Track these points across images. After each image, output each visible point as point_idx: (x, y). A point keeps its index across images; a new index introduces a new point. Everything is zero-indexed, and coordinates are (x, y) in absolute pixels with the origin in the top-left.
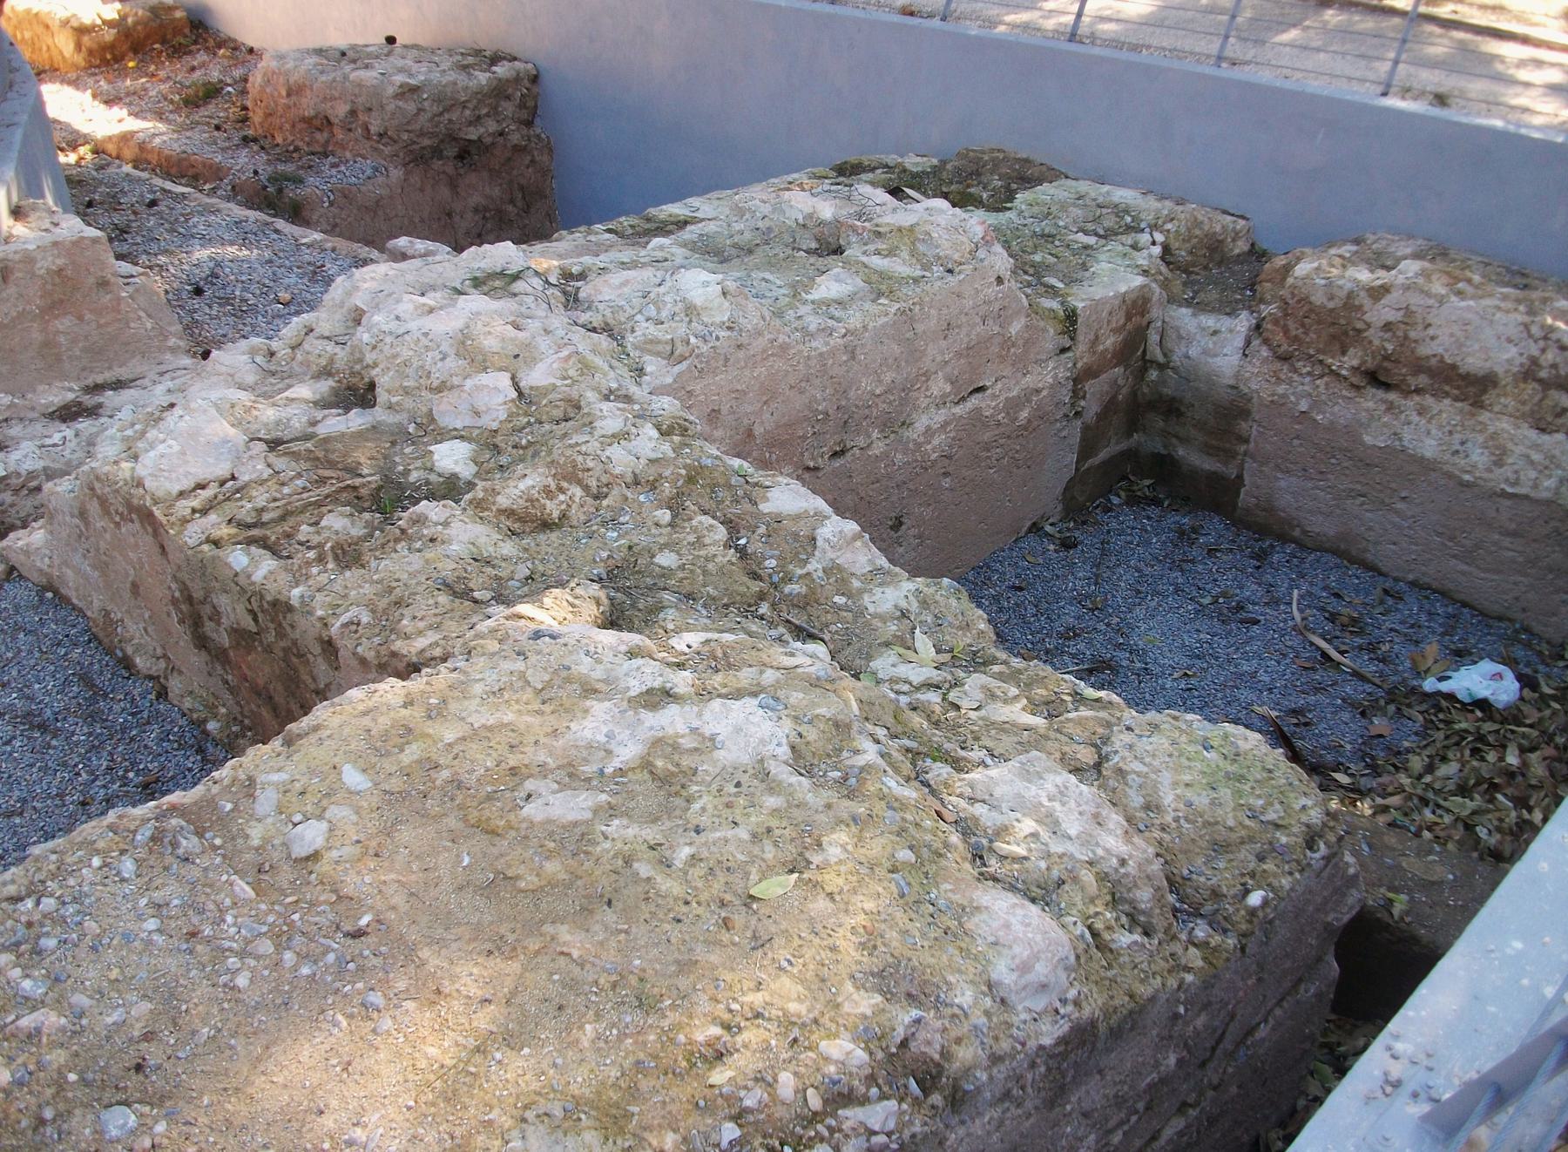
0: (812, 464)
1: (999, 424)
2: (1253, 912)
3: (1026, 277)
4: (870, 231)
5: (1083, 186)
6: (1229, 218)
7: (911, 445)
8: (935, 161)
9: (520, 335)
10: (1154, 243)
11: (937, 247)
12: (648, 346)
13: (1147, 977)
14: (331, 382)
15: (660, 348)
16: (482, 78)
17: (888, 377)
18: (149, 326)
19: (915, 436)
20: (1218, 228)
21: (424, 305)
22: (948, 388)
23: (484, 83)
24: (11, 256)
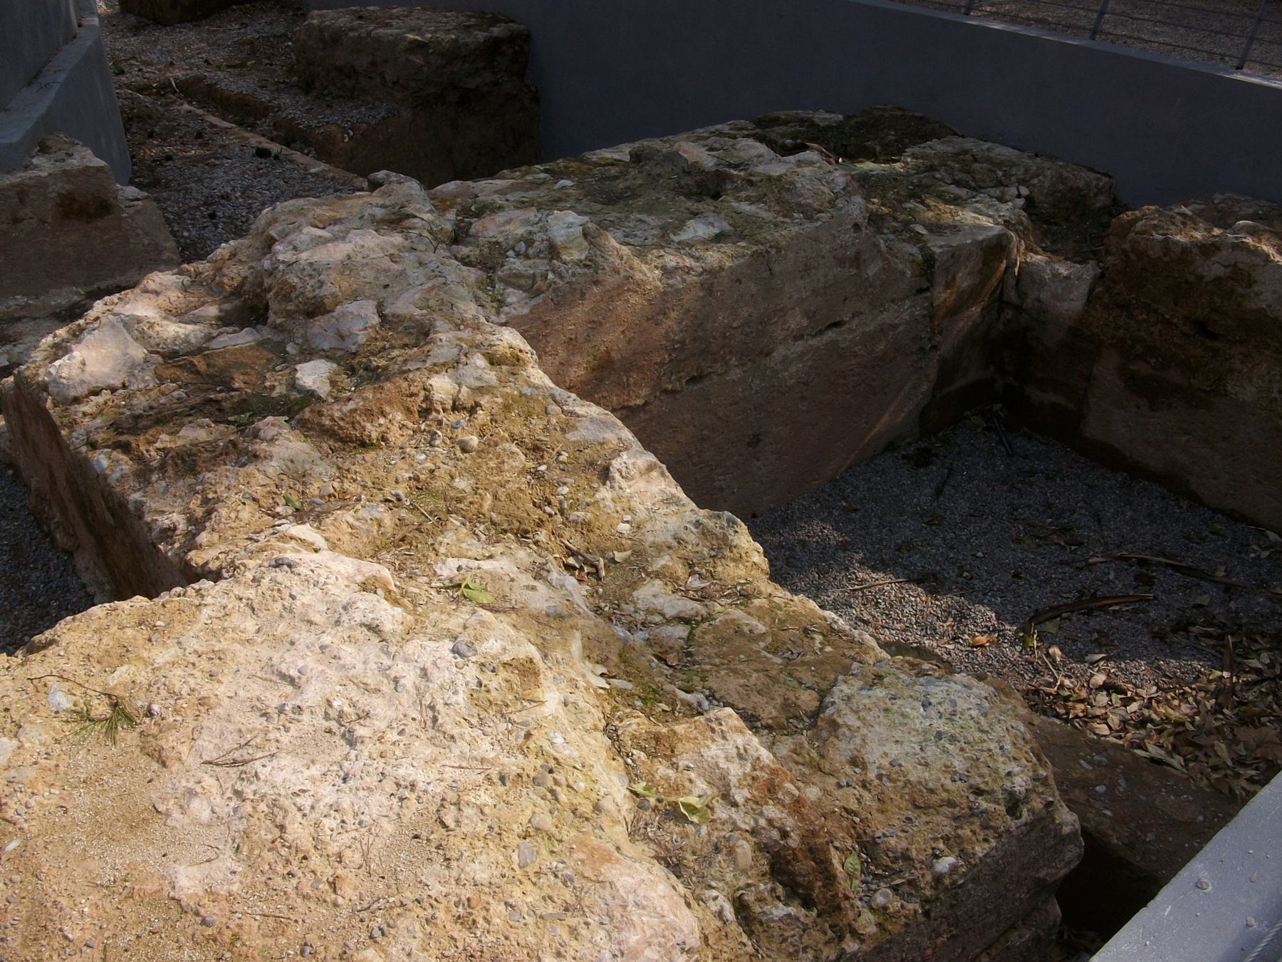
0: (670, 387)
1: (855, 355)
2: (938, 879)
3: (895, 224)
4: (743, 179)
5: (969, 144)
6: (1093, 175)
7: (768, 372)
8: (841, 117)
9: (395, 266)
10: (1019, 196)
11: (800, 196)
12: (512, 280)
13: (797, 952)
14: (236, 302)
15: (523, 282)
16: (481, 36)
17: (745, 312)
18: (146, 242)
19: (772, 364)
20: (1081, 184)
21: (320, 237)
22: (805, 322)
23: (482, 40)
24: (27, 181)
